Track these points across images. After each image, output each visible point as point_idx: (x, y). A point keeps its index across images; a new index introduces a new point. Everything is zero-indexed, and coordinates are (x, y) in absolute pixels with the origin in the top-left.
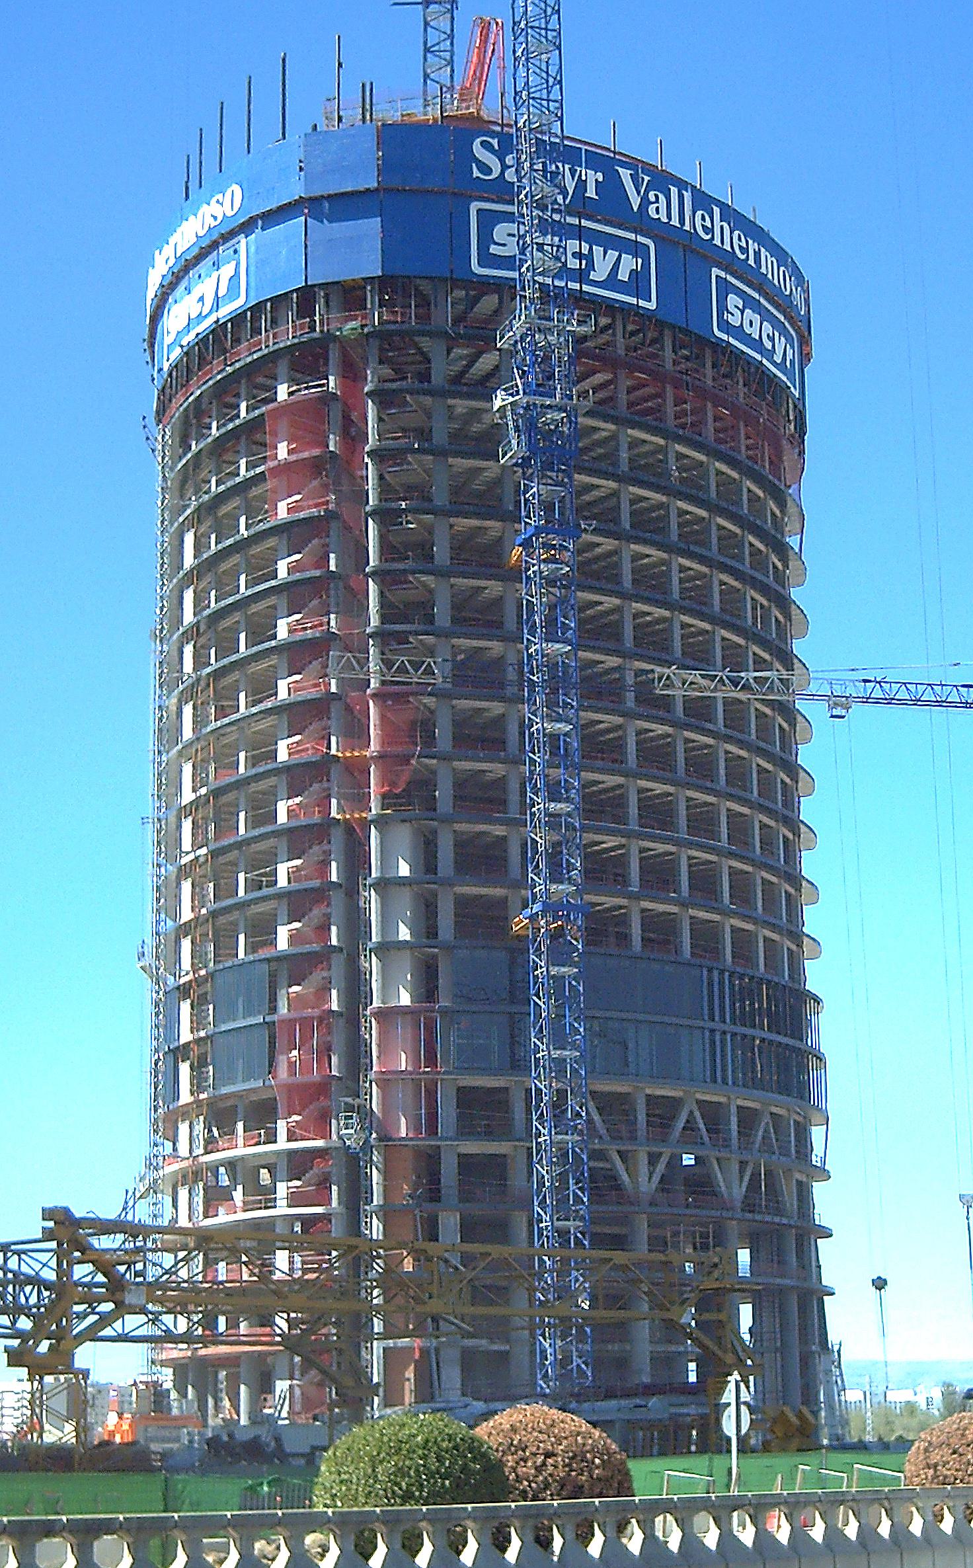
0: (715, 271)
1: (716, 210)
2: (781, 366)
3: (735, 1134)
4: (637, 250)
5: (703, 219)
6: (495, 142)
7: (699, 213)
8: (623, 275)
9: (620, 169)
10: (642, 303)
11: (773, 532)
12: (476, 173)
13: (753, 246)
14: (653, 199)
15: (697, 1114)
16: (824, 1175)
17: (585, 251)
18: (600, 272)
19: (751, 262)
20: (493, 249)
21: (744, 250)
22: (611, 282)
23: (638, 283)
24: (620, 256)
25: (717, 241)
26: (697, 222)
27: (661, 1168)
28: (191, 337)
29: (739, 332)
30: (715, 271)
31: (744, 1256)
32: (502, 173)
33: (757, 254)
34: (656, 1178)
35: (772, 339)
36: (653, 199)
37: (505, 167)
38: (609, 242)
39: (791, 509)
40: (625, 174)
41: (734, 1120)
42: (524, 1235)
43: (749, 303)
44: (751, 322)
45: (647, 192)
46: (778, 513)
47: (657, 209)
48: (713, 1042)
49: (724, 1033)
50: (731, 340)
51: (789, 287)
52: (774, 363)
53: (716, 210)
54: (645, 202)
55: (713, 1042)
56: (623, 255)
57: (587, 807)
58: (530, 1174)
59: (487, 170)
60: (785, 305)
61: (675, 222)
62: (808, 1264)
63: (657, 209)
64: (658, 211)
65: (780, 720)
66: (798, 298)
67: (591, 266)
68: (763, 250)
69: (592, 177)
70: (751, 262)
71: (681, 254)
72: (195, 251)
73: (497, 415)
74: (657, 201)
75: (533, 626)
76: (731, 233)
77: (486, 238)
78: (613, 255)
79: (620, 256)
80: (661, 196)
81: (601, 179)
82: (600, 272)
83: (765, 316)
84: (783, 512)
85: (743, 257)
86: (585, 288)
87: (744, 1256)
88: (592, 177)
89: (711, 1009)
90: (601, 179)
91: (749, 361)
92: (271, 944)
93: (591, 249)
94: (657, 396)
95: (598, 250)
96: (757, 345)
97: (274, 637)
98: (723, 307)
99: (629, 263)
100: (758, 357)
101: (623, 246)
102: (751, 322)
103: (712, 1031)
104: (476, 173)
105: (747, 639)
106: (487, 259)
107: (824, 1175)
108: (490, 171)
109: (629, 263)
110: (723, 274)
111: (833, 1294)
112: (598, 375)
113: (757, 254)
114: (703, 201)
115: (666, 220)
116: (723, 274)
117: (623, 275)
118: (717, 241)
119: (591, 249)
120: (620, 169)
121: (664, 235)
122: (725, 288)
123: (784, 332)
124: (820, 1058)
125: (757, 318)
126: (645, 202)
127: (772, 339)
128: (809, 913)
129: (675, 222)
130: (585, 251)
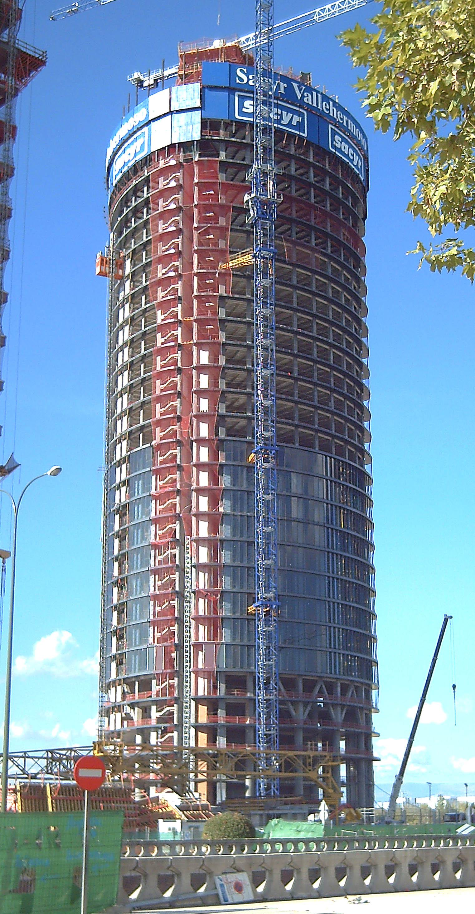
0: (330, 126)
1: (331, 103)
2: (357, 166)
3: (339, 694)
4: (300, 114)
5: (326, 105)
6: (245, 70)
7: (324, 103)
8: (294, 123)
9: (294, 84)
10: (301, 134)
11: (356, 377)
12: (238, 81)
13: (345, 118)
14: (306, 95)
15: (324, 686)
16: (377, 711)
17: (280, 112)
18: (285, 121)
19: (345, 124)
20: (244, 110)
21: (342, 119)
22: (289, 125)
23: (300, 126)
24: (293, 116)
25: (331, 114)
26: (323, 106)
27: (309, 708)
28: (126, 169)
29: (339, 150)
30: (330, 126)
31: (342, 744)
32: (248, 81)
33: (347, 122)
34: (307, 713)
35: (353, 156)
36: (306, 95)
37: (249, 80)
38: (289, 110)
39: (366, 413)
40: (295, 85)
41: (339, 689)
42: (252, 737)
43: (343, 139)
44: (345, 147)
45: (303, 93)
46: (359, 391)
47: (308, 100)
48: (328, 557)
49: (335, 653)
50: (337, 153)
51: (360, 137)
52: (353, 165)
53: (331, 103)
54: (303, 96)
55: (328, 557)
56: (294, 116)
57: (278, 372)
58: (255, 711)
59: (242, 80)
60: (358, 144)
61: (315, 105)
62: (369, 747)
63: (308, 100)
64: (308, 100)
65: (355, 324)
66: (363, 142)
67: (281, 118)
68: (349, 121)
69: (283, 85)
70: (345, 124)
71: (317, 119)
72: (128, 136)
73: (245, 204)
74: (308, 96)
75: (258, 364)
76: (337, 112)
77: (241, 106)
78: (290, 115)
79: (293, 116)
80: (309, 95)
81: (286, 86)
82: (285, 121)
83: (350, 146)
84: (362, 413)
85: (342, 122)
86: (279, 126)
87: (342, 744)
88: (283, 85)
89: (329, 569)
90: (286, 86)
91: (343, 162)
92: (140, 238)
93: (282, 112)
94: (307, 236)
95: (284, 113)
96: (347, 156)
97: (156, 323)
98: (333, 140)
99: (296, 119)
100: (348, 161)
101: (294, 112)
102: (345, 147)
103: (330, 652)
104: (238, 81)
105: (344, 376)
106: (241, 113)
107: (377, 711)
108: (243, 81)
109: (296, 119)
110: (333, 127)
111: (379, 760)
112: (285, 226)
113: (347, 122)
114: (326, 98)
115: (311, 104)
116: (333, 127)
117: (294, 123)
118: (331, 114)
119: (282, 112)
120: (294, 84)
121: (310, 109)
122: (334, 133)
123: (357, 154)
124: (373, 569)
125: (347, 146)
126: (303, 96)
127: (353, 156)
128: (374, 717)
129: (315, 105)
130: (280, 112)
